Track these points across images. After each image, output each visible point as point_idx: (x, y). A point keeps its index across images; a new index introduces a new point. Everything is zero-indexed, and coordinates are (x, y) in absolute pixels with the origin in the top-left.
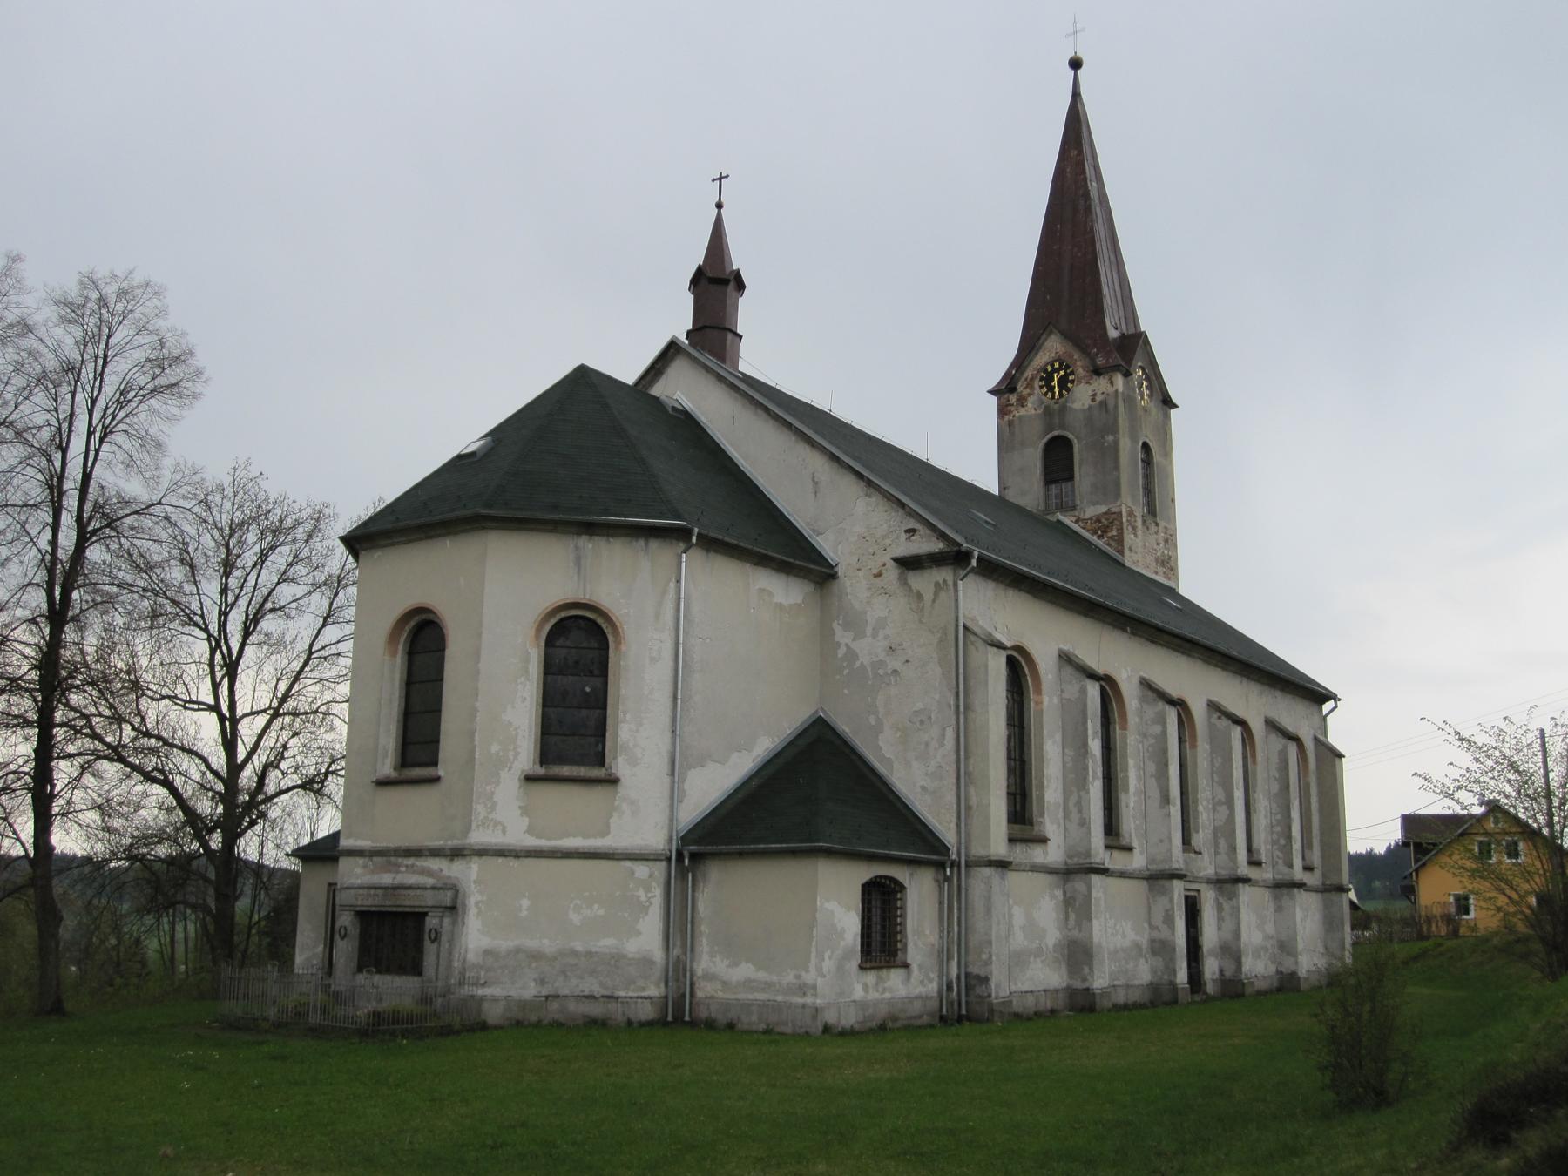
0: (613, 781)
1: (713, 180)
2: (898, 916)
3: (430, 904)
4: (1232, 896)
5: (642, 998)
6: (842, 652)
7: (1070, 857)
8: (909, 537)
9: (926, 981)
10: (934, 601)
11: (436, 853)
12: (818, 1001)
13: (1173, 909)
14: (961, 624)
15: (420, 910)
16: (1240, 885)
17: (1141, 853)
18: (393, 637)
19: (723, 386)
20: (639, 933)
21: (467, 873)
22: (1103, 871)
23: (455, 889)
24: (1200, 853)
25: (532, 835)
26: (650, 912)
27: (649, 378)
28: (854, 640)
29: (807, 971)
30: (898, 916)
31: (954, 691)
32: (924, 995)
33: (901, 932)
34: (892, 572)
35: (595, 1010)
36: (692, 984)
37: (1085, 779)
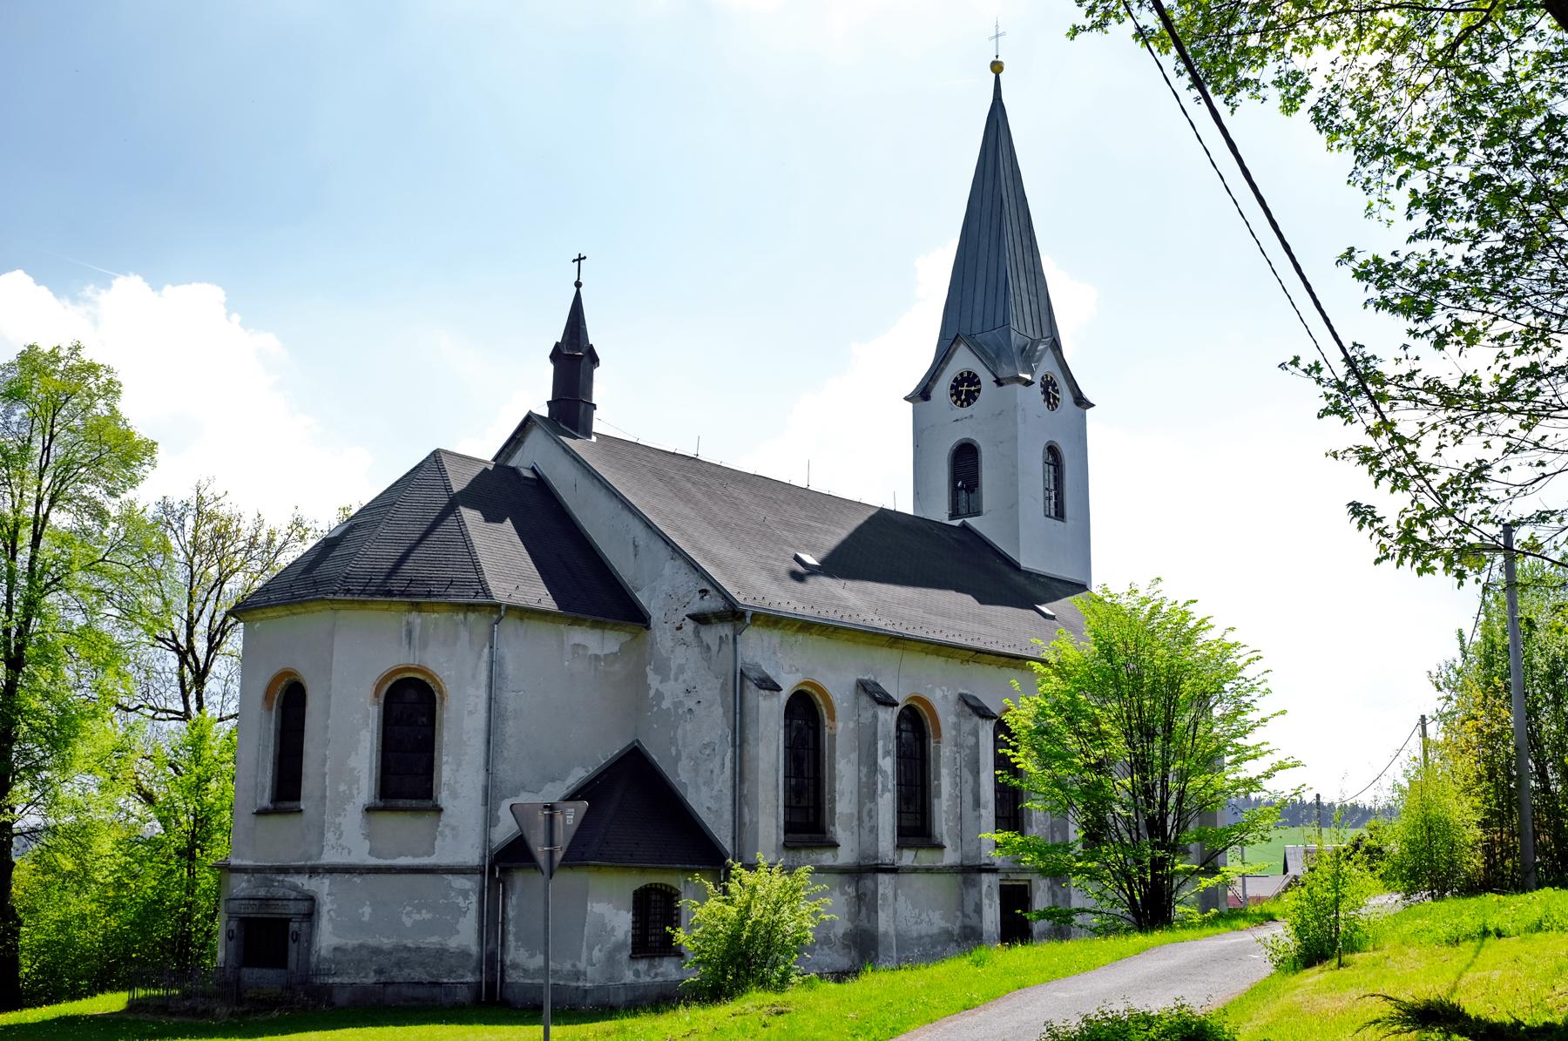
1: (574, 261)
3: (292, 912)
5: (461, 983)
6: (652, 693)
7: (864, 858)
8: (702, 597)
11: (299, 870)
13: (981, 899)
14: (739, 671)
17: (955, 851)
21: (321, 887)
22: (893, 870)
23: (311, 899)
26: (468, 915)
28: (661, 682)
34: (689, 626)
35: (420, 992)
36: (503, 971)
37: (875, 792)
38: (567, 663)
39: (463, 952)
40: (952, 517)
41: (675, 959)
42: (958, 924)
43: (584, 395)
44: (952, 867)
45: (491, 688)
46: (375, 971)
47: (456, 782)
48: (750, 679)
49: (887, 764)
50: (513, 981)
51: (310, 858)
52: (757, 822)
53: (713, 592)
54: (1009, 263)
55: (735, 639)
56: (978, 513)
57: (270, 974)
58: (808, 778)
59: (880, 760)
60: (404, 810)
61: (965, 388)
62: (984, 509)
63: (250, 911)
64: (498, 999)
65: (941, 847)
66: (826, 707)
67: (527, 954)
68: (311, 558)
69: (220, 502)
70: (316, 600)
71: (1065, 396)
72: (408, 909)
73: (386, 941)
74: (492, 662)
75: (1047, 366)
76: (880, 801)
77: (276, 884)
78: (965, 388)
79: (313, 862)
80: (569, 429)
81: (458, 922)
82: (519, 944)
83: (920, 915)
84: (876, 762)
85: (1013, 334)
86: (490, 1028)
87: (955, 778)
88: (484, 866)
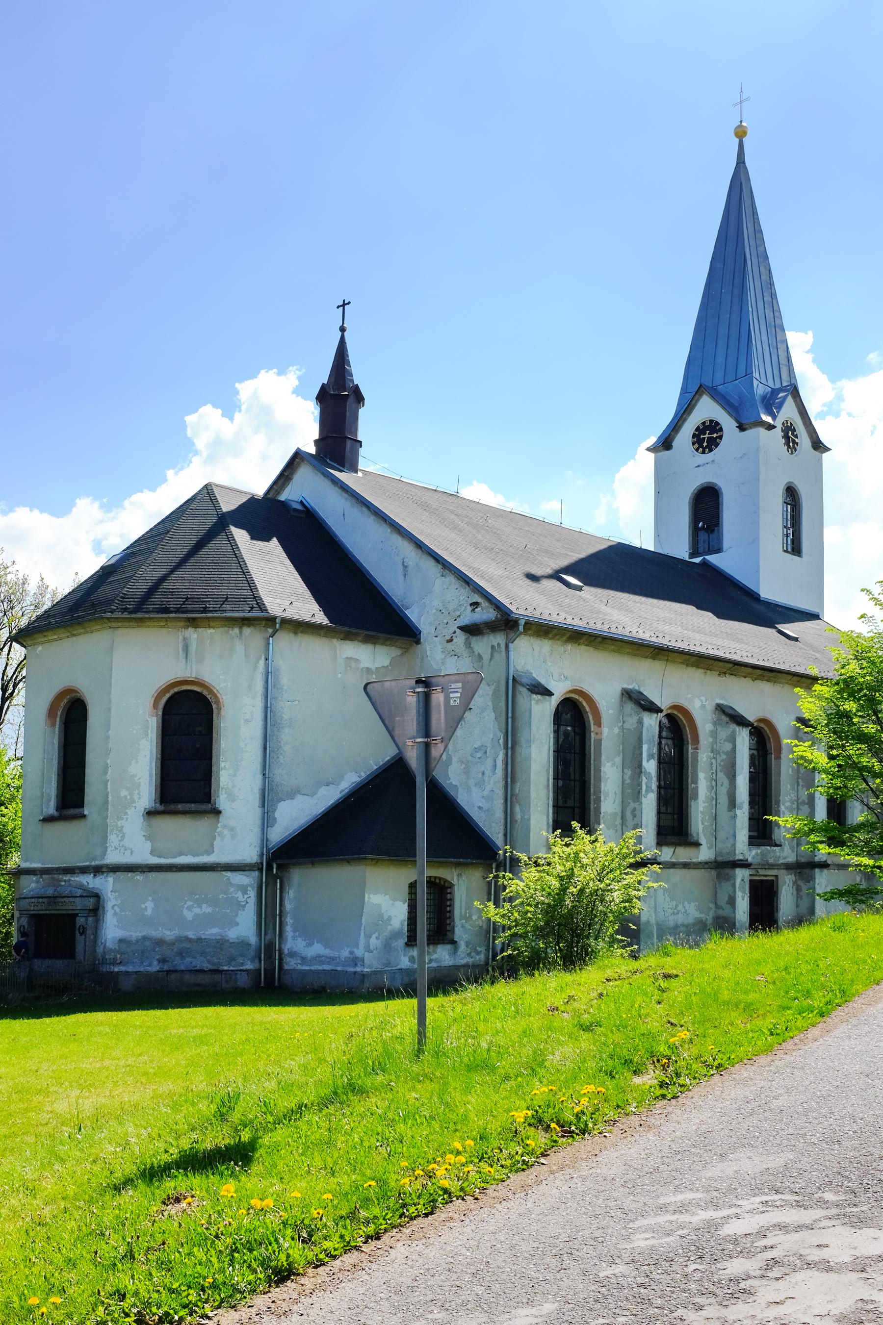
0: (217, 812)
1: (338, 307)
2: (448, 906)
4: (811, 879)
5: (241, 970)
8: (473, 610)
9: (473, 954)
10: (491, 659)
11: (84, 870)
12: (366, 970)
13: (735, 892)
14: (511, 678)
15: (73, 912)
16: (817, 870)
17: (709, 848)
18: (51, 712)
19: (336, 488)
20: (237, 924)
21: (106, 884)
23: (97, 896)
24: (780, 846)
25: (154, 856)
27: (280, 483)
29: (358, 948)
30: (448, 906)
31: (504, 731)
32: (471, 963)
33: (450, 918)
34: (461, 638)
35: (205, 979)
36: (281, 959)
38: (340, 676)
39: (242, 942)
40: (693, 555)
41: (449, 947)
42: (711, 914)
43: (351, 433)
44: (706, 863)
45: (266, 697)
46: (159, 960)
47: (233, 787)
48: (523, 685)
49: (651, 766)
50: (292, 968)
51: (94, 859)
52: (529, 819)
53: (484, 603)
54: (752, 317)
55: (507, 647)
56: (719, 550)
57: (60, 963)
58: (575, 780)
59: (644, 763)
60: (184, 813)
61: (707, 436)
62: (725, 545)
63: (41, 908)
64: (276, 984)
65: (697, 844)
66: (593, 714)
67: (304, 943)
68: (89, 585)
69: (8, 570)
70: (95, 619)
71: (804, 440)
72: (189, 903)
73: (168, 933)
74: (267, 673)
75: (788, 411)
76: (644, 800)
77: (63, 883)
78: (707, 436)
79: (97, 863)
80: (335, 465)
81: (237, 915)
82: (297, 933)
83: (677, 906)
84: (640, 765)
85: (755, 383)
86: (274, 1008)
87: (711, 782)
88: (262, 863)
